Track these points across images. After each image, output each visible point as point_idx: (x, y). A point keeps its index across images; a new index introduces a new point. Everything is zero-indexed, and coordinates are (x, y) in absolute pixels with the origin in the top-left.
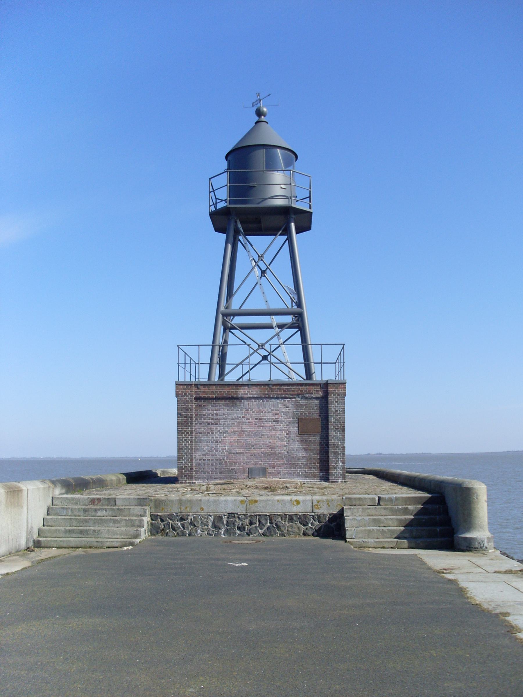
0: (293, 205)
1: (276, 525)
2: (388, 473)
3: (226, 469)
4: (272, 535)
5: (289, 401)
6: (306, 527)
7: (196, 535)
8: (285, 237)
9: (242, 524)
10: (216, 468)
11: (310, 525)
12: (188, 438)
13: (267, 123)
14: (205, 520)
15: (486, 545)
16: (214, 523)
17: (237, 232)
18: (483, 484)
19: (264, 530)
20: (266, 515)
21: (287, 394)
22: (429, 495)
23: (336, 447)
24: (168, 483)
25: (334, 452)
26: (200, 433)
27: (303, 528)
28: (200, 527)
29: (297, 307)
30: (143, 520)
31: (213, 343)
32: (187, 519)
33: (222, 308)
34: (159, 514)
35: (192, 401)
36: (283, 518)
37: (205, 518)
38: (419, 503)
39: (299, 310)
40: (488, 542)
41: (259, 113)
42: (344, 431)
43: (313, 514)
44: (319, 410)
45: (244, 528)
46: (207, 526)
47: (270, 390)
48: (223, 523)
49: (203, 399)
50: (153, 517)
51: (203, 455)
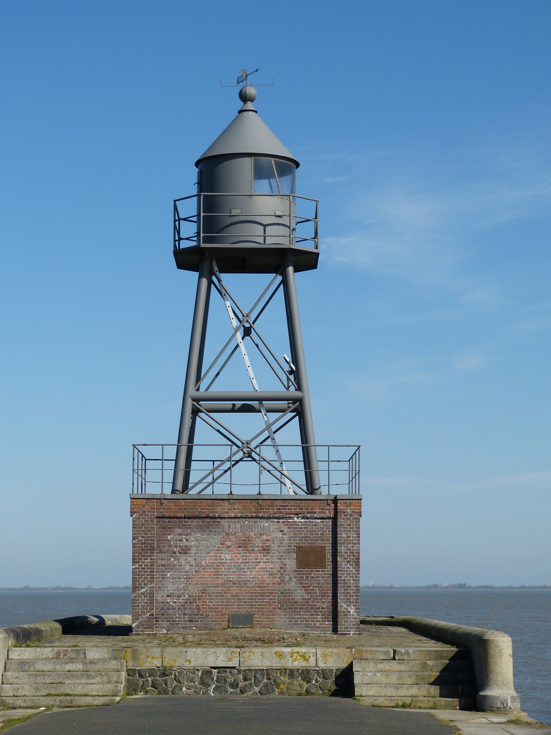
0: (292, 247)
1: (275, 681)
2: (421, 624)
3: (198, 615)
4: (269, 693)
5: (284, 522)
6: (309, 684)
7: (181, 693)
8: (280, 278)
9: (235, 680)
10: (185, 614)
11: (314, 682)
12: (147, 572)
13: (256, 112)
14: (192, 675)
15: (509, 704)
16: (202, 678)
17: (212, 273)
18: (507, 636)
19: (260, 687)
20: (263, 670)
21: (282, 513)
22: (457, 649)
23: (348, 587)
24: (119, 635)
25: (344, 593)
26: (162, 565)
27: (305, 685)
28: (186, 683)
29: (296, 390)
30: (122, 675)
31: (179, 441)
32: (171, 674)
33: (192, 392)
34: (137, 668)
35: (153, 522)
36: (283, 673)
37: (192, 673)
38: (443, 658)
39: (298, 394)
40: (512, 702)
41: (244, 98)
42: (358, 564)
43: (317, 669)
44: (325, 532)
45: (237, 685)
46: (194, 682)
47: (258, 507)
48: (213, 679)
49: (167, 518)
50: (130, 673)
51: (167, 596)
